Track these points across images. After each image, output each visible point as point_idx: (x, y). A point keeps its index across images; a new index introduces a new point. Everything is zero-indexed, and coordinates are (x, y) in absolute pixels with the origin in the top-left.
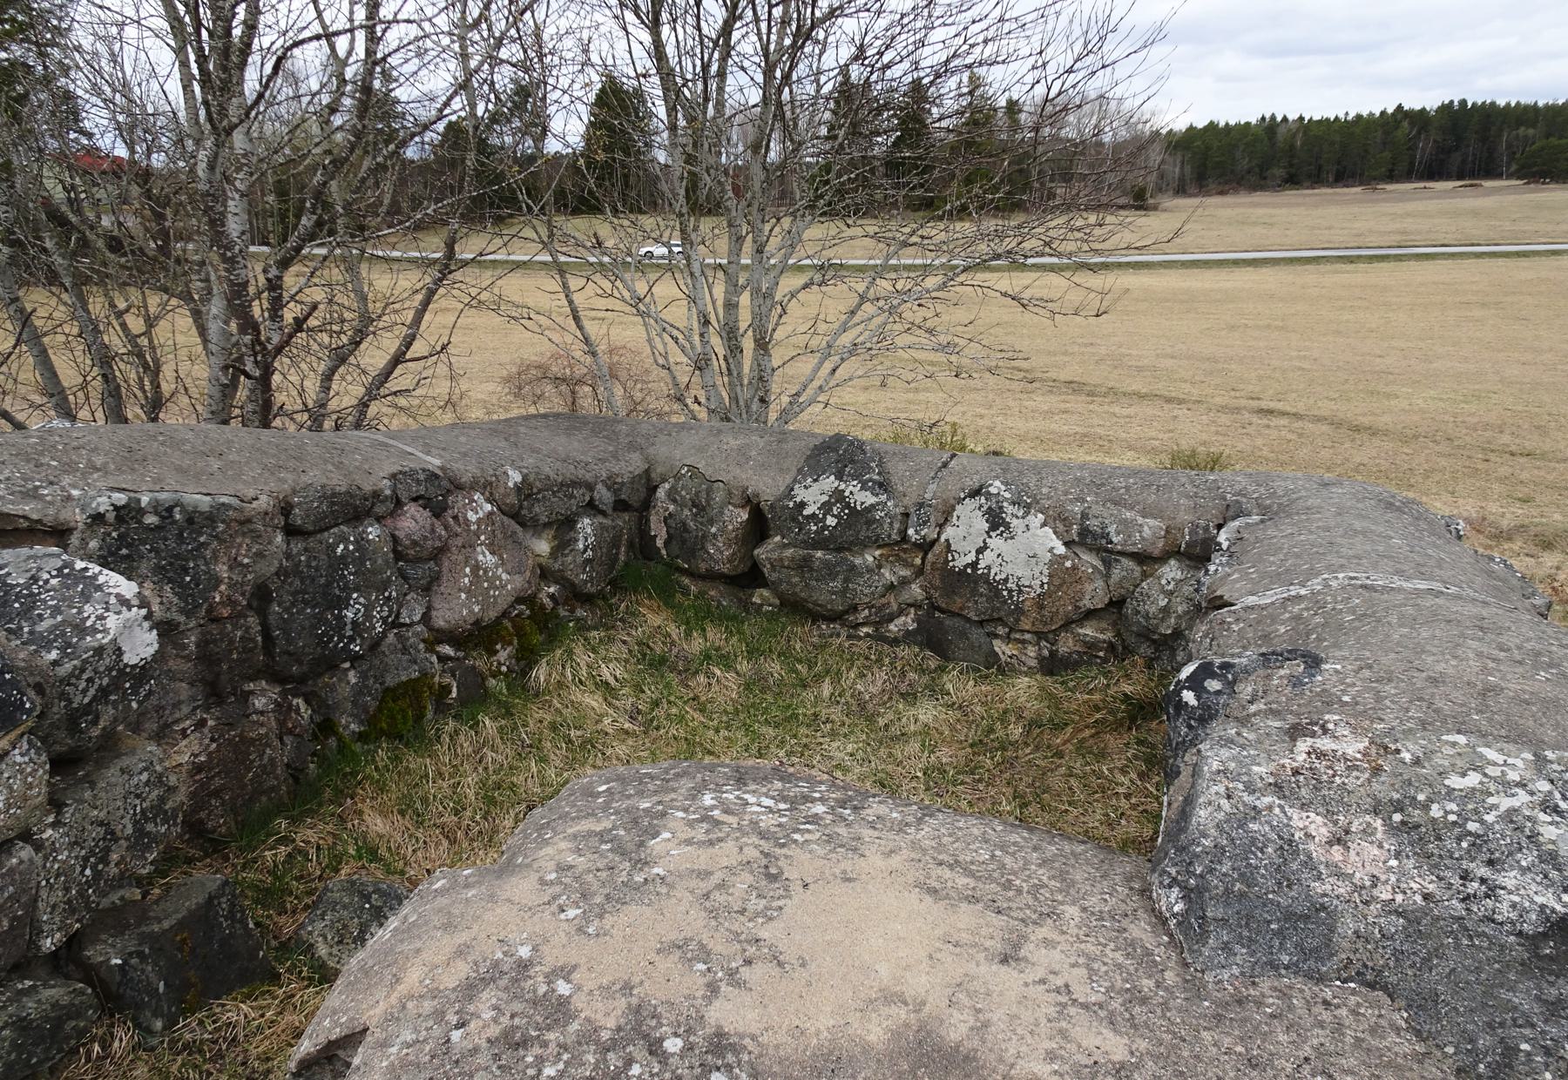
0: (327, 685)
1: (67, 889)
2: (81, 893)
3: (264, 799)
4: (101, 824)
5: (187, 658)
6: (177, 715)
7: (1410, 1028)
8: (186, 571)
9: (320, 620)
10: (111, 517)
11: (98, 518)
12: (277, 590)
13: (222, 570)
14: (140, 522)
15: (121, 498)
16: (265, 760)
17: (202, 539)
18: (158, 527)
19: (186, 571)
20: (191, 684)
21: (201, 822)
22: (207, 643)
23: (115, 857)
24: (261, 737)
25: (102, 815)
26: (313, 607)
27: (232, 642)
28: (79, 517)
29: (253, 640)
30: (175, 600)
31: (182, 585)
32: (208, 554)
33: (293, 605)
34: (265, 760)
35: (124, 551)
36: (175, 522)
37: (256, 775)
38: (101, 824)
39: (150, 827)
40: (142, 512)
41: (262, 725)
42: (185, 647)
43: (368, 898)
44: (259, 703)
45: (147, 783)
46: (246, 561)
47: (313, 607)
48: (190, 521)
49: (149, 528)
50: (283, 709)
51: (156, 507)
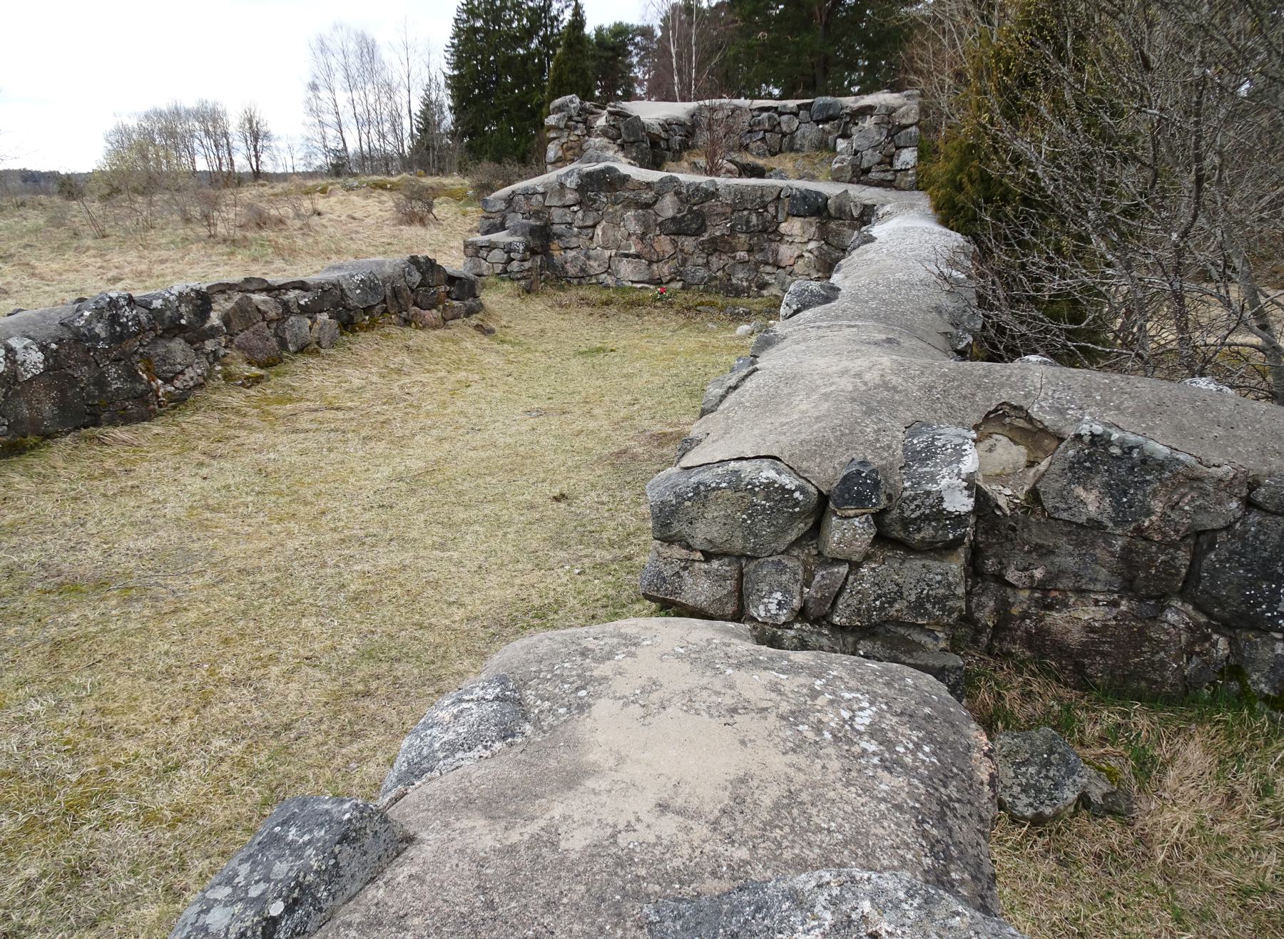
0: (1249, 640)
1: (860, 603)
2: (868, 610)
3: (1143, 684)
4: (897, 585)
5: (1113, 554)
6: (1091, 587)
7: (525, 717)
8: (1125, 493)
9: (1252, 584)
10: (1087, 439)
11: (1079, 437)
12: (1221, 544)
13: (1157, 506)
14: (1106, 449)
15: (1098, 429)
16: (1156, 658)
17: (1148, 478)
18: (1118, 458)
19: (1125, 493)
20: (1112, 573)
21: (1084, 665)
22: (1131, 551)
23: (897, 606)
24: (1159, 641)
25: (900, 581)
26: (1248, 571)
27: (1152, 560)
28: (1070, 432)
29: (1178, 570)
30: (1110, 510)
31: (1119, 502)
32: (1149, 489)
33: (1228, 560)
34: (1156, 658)
35: (1087, 464)
36: (1131, 458)
37: (1142, 663)
38: (897, 585)
39: (929, 606)
40: (1110, 443)
41: (1168, 634)
42: (1111, 545)
43: (1051, 752)
44: (1171, 617)
45: (939, 582)
46: (1187, 508)
47: (1248, 571)
48: (1144, 462)
49: (1111, 456)
50: (1198, 635)
51: (1121, 444)
